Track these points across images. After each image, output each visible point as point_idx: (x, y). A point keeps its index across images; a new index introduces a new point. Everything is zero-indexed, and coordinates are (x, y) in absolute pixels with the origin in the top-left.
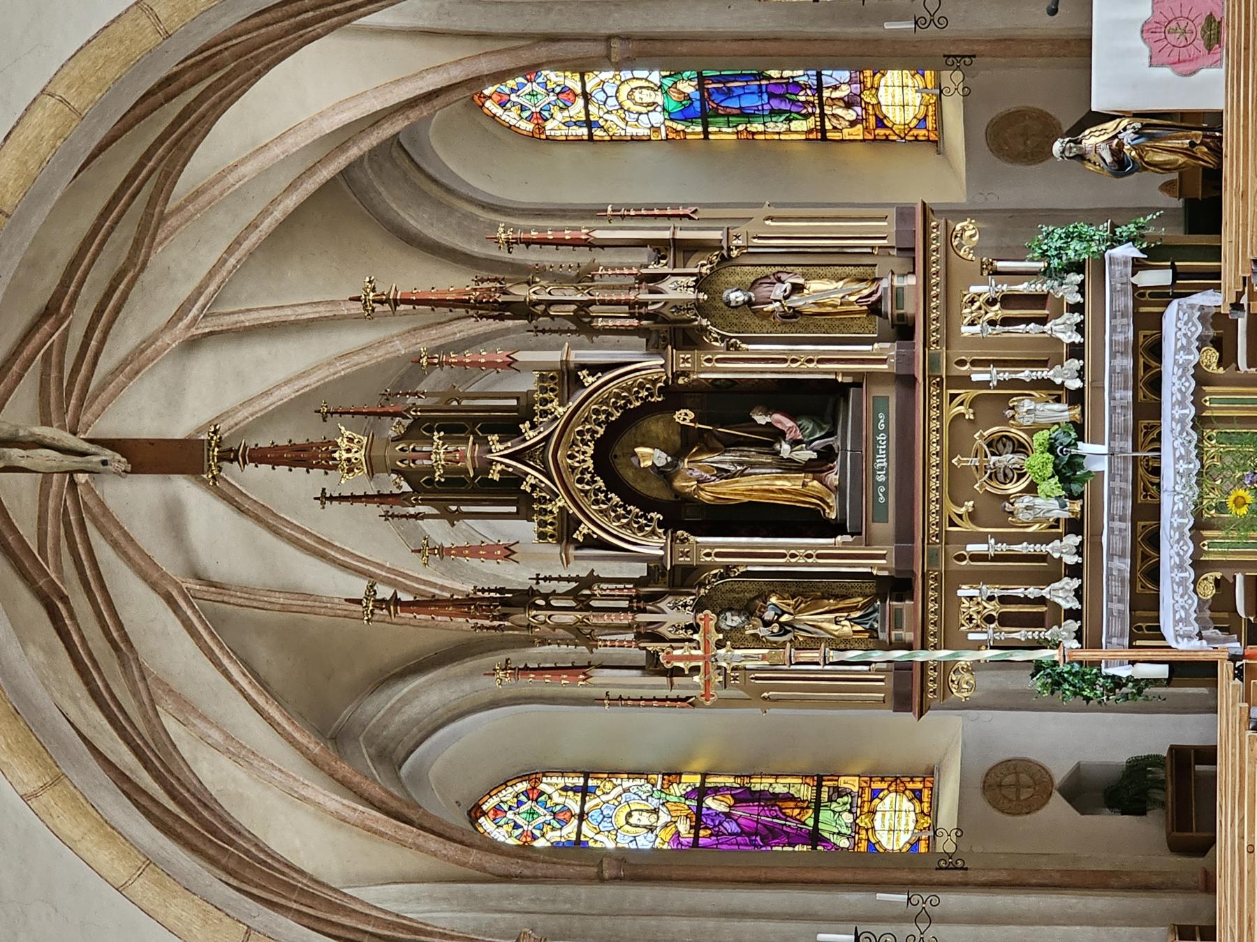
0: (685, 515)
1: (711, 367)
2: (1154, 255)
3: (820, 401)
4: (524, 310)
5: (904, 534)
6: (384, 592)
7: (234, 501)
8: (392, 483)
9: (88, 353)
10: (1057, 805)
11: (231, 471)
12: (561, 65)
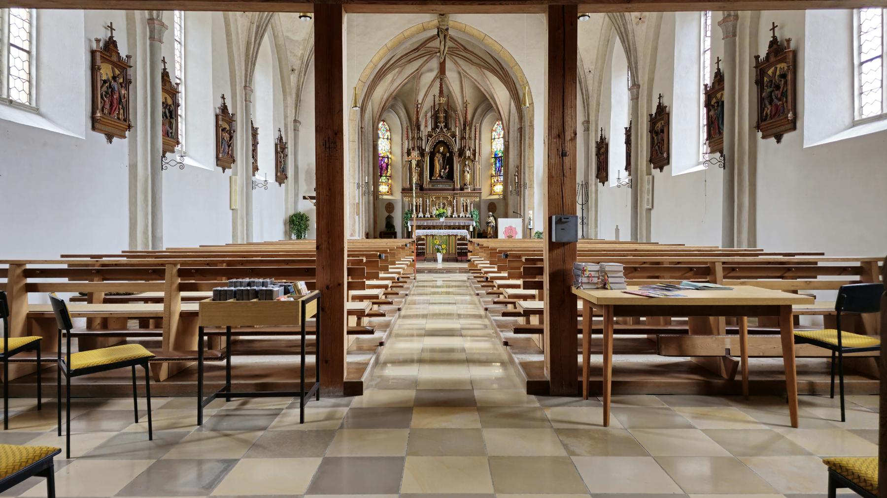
1: (456, 159)
2: (474, 228)
3: (450, 176)
4: (465, 128)
5: (430, 190)
7: (434, 80)
9: (458, 55)
11: (438, 80)
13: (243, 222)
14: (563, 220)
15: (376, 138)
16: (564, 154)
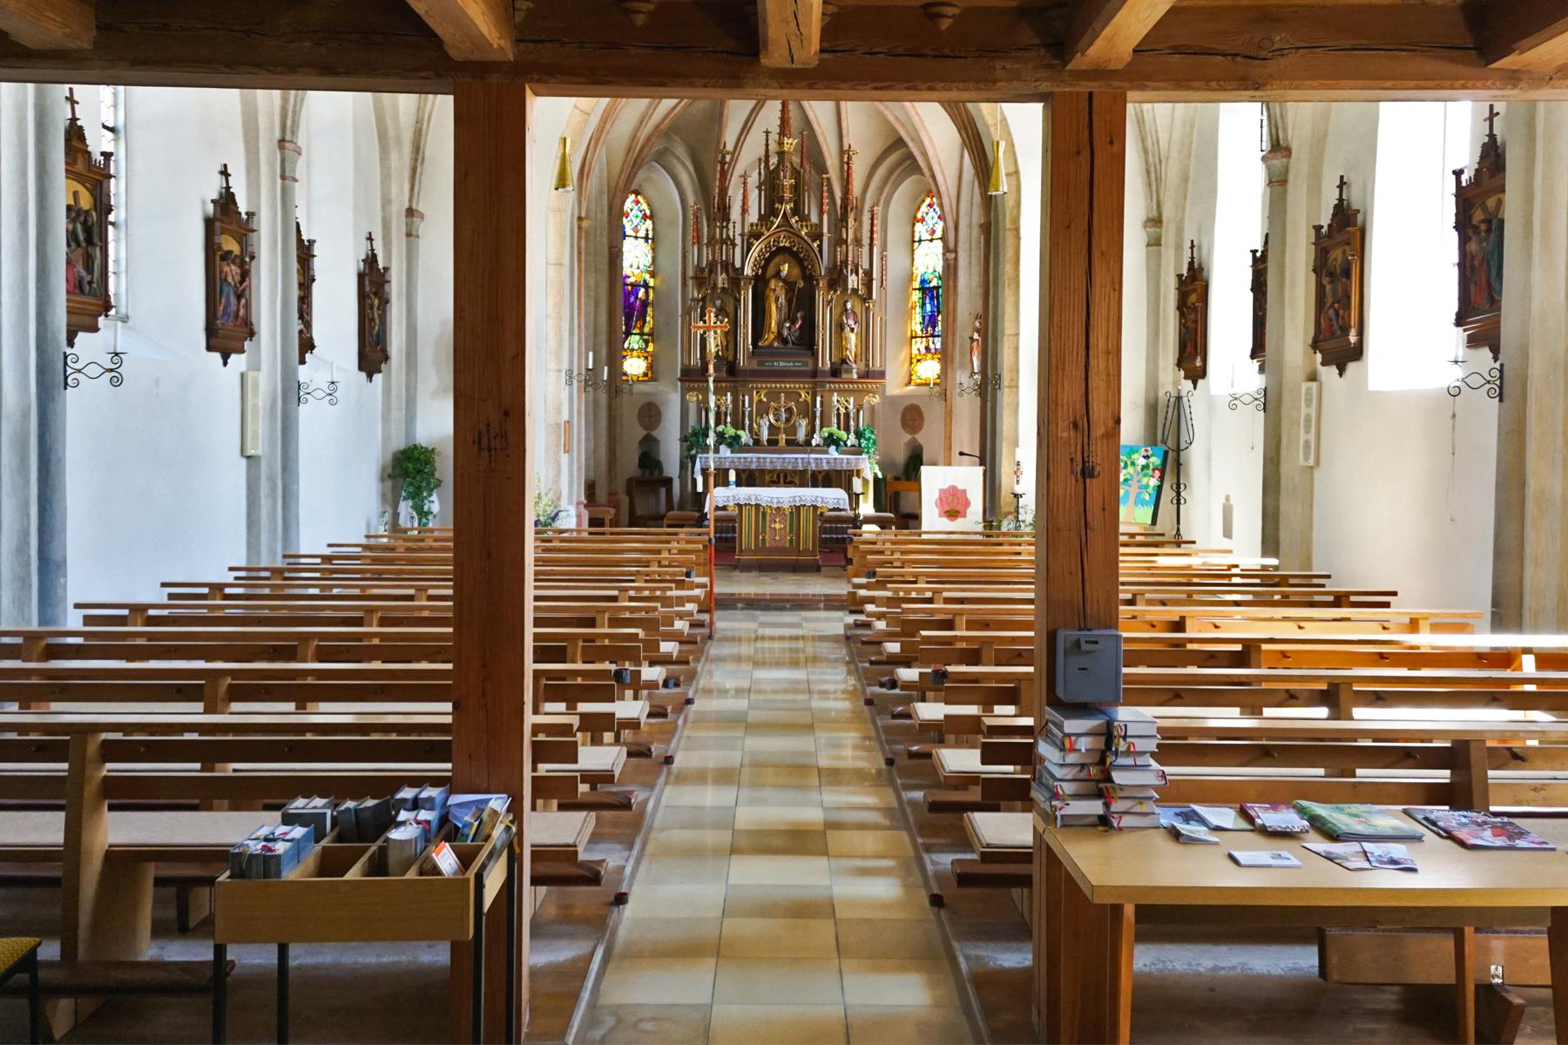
0: (760, 283)
3: (807, 339)
6: (728, 158)
8: (774, 160)
10: (642, 433)
12: (945, 231)
13: (273, 489)
14: (1085, 647)
15: (617, 235)
16: (1087, 473)
